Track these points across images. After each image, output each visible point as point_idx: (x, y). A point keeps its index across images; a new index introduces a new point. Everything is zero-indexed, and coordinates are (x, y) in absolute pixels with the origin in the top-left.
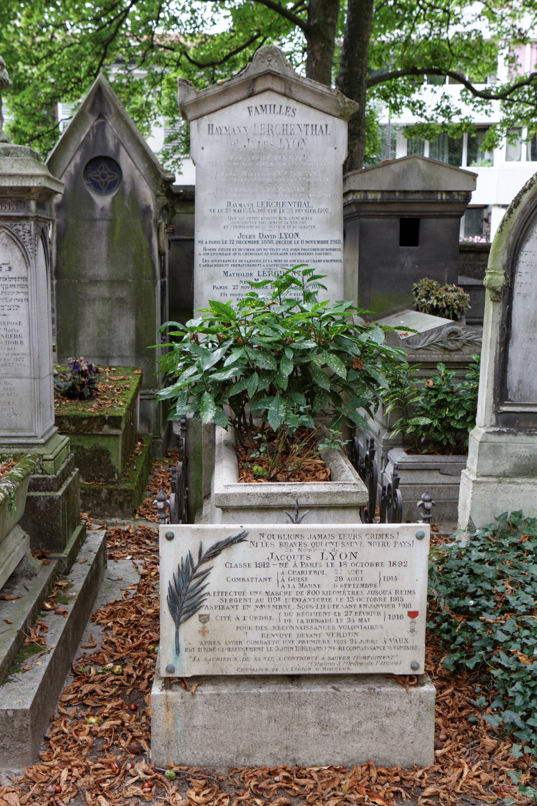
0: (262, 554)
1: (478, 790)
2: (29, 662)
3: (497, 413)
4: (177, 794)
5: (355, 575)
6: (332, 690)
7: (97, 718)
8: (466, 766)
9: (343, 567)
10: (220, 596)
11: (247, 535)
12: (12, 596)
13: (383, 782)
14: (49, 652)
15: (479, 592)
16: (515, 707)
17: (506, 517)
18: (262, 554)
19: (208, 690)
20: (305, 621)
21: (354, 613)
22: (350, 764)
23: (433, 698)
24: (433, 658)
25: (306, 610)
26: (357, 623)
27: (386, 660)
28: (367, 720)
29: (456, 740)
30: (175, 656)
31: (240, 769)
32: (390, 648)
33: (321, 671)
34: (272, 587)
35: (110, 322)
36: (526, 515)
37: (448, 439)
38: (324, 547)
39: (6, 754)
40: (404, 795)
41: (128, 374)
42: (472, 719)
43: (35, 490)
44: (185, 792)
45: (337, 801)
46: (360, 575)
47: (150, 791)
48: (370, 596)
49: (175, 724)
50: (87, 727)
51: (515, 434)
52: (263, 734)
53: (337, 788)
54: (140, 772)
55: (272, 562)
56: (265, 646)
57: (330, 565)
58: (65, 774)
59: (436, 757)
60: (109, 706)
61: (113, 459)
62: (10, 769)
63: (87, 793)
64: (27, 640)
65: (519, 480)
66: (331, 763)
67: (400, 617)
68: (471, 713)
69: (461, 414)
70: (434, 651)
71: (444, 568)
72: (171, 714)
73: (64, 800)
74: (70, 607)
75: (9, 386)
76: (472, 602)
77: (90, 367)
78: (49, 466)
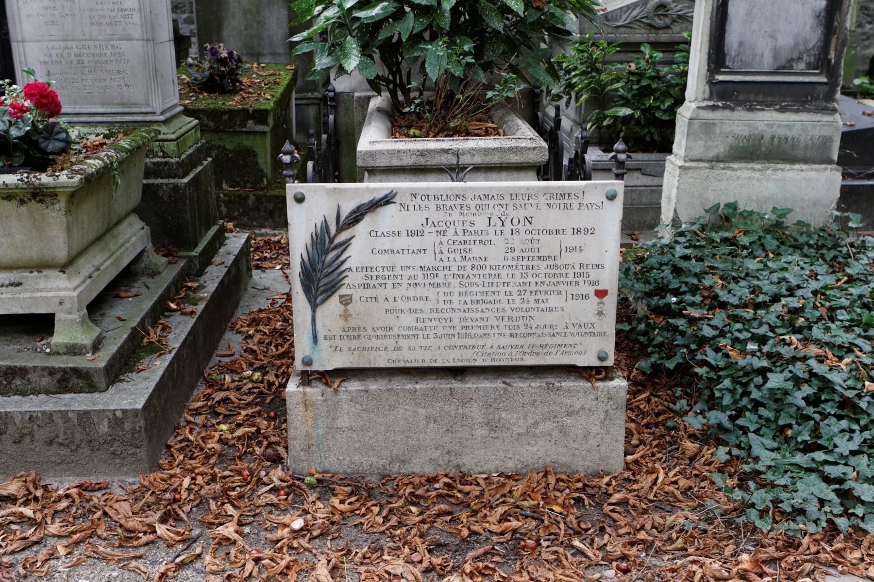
0: (414, 220)
1: (675, 497)
2: (145, 362)
3: (711, 83)
4: (318, 502)
5: (530, 246)
6: (502, 385)
7: (228, 425)
8: (662, 471)
9: (515, 236)
10: (364, 273)
11: (395, 195)
12: (130, 294)
13: (562, 489)
14: (170, 352)
15: (684, 288)
16: (722, 406)
17: (719, 208)
18: (414, 220)
19: (353, 386)
20: (469, 302)
21: (528, 293)
22: (524, 471)
23: (624, 395)
24: (627, 342)
25: (469, 289)
26: (532, 304)
27: (568, 349)
28: (544, 420)
29: (651, 444)
30: (312, 345)
31: (393, 476)
32: (572, 334)
33: (488, 363)
34: (427, 260)
35: (258, 12)
36: (741, 207)
37: (652, 134)
38: (491, 210)
39: (117, 461)
40: (586, 502)
41: (280, 70)
42: (670, 424)
43: (156, 177)
44: (328, 500)
45: (507, 508)
46: (536, 246)
47: (286, 499)
48: (549, 271)
49: (315, 426)
50: (217, 435)
51: (733, 109)
52: (421, 436)
53: (508, 495)
54: (275, 479)
55: (427, 230)
56: (420, 333)
57: (498, 232)
58: (187, 482)
59: (626, 463)
60: (244, 413)
61: (261, 161)
62: (123, 478)
63: (211, 501)
64: (145, 340)
65: (735, 165)
66: (501, 470)
67: (586, 297)
68: (670, 418)
69: (668, 103)
70: (628, 357)
71: (643, 268)
72: (310, 414)
73: (184, 509)
74: (201, 307)
75: (117, 50)
76: (674, 299)
77: (231, 54)
78: (171, 147)
